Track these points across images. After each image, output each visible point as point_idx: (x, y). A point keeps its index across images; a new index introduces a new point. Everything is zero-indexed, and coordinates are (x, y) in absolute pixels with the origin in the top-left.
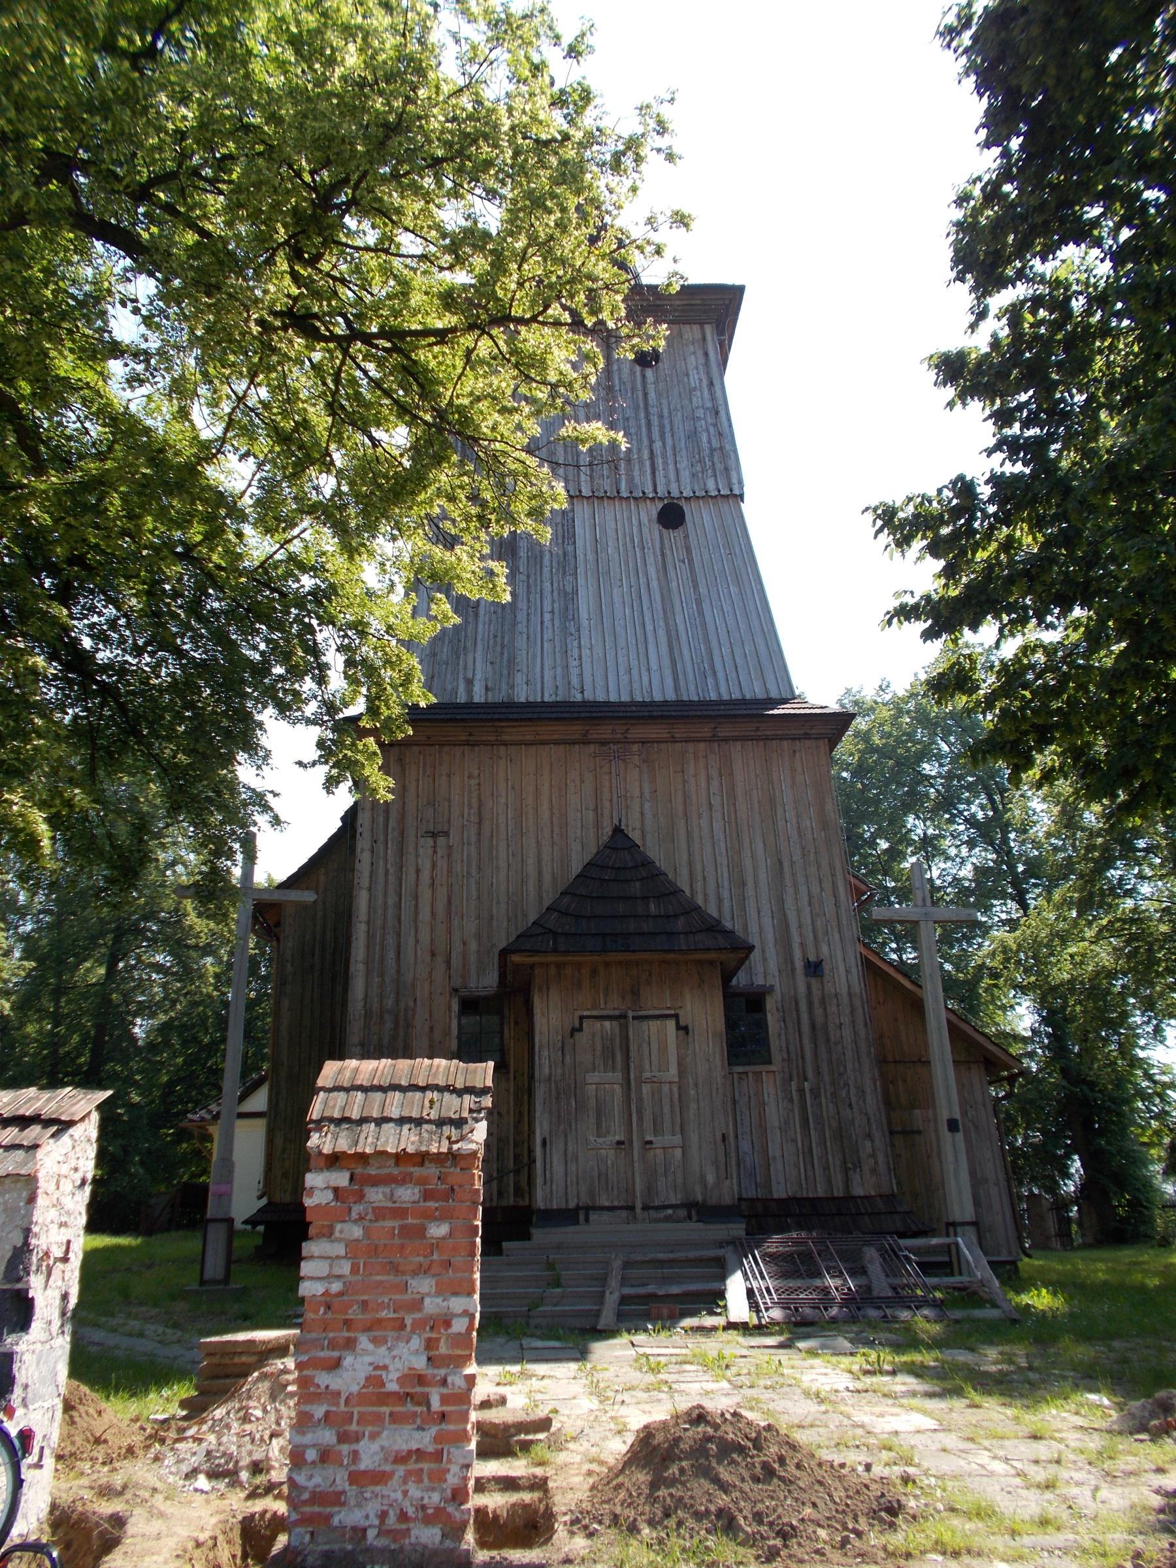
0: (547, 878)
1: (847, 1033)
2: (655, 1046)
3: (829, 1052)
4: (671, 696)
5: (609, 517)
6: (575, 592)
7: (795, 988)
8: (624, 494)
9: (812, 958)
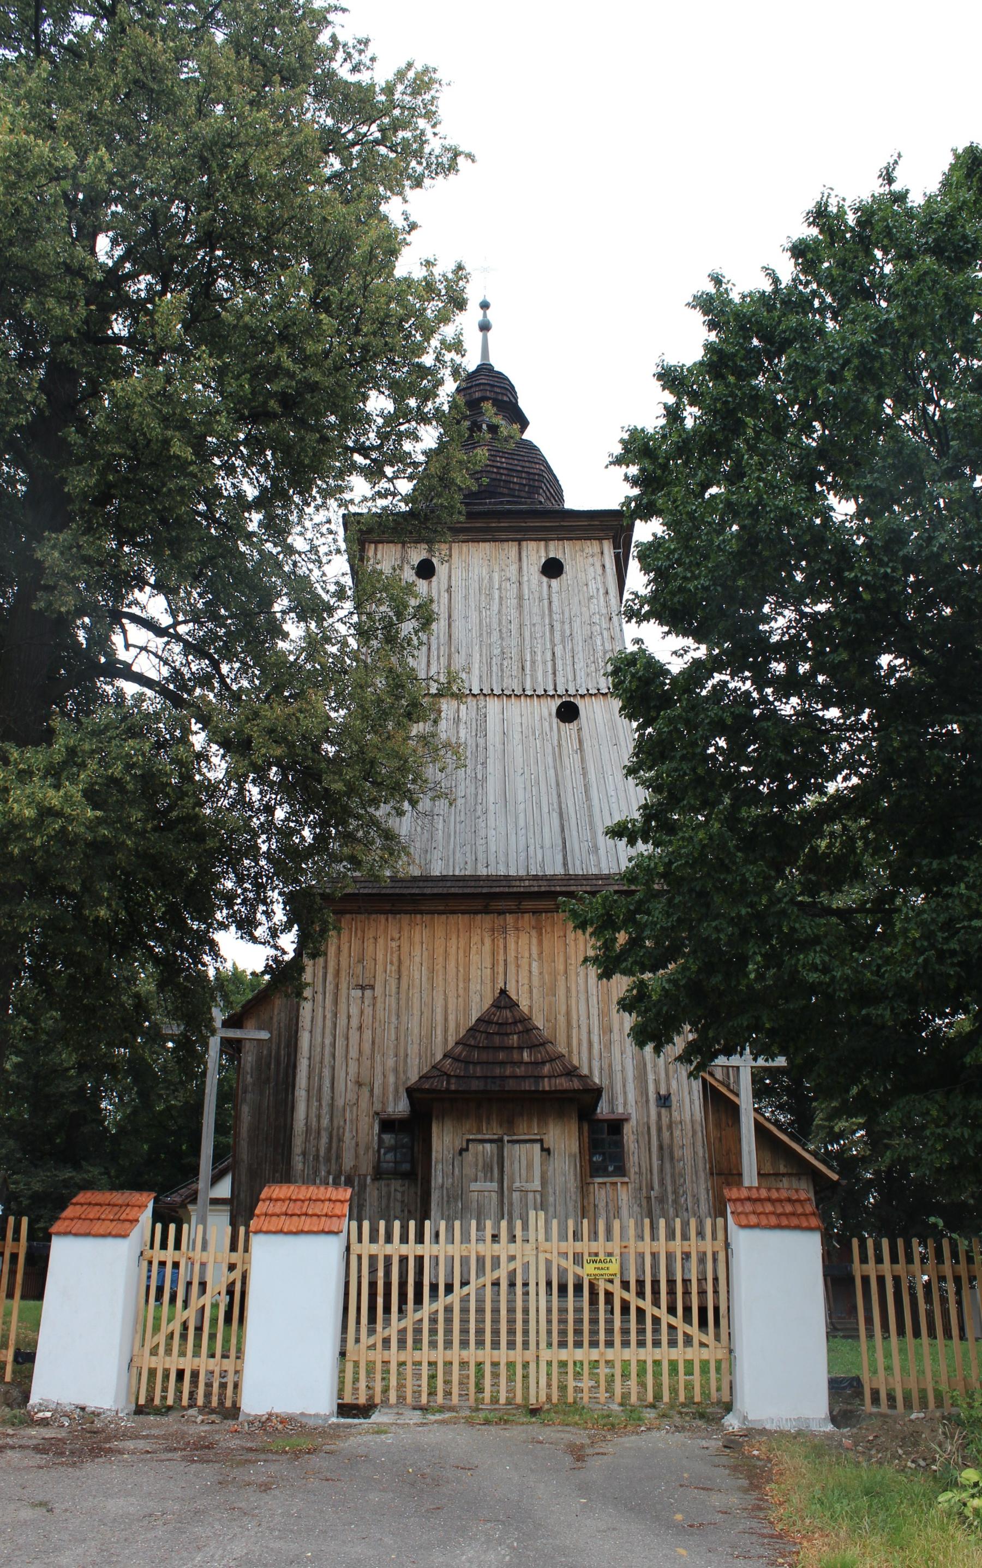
0: (452, 1025)
1: (688, 1153)
2: (524, 1163)
3: (673, 1167)
4: (560, 870)
5: (516, 711)
6: (485, 779)
7: (648, 1116)
8: (529, 693)
9: (663, 1092)
